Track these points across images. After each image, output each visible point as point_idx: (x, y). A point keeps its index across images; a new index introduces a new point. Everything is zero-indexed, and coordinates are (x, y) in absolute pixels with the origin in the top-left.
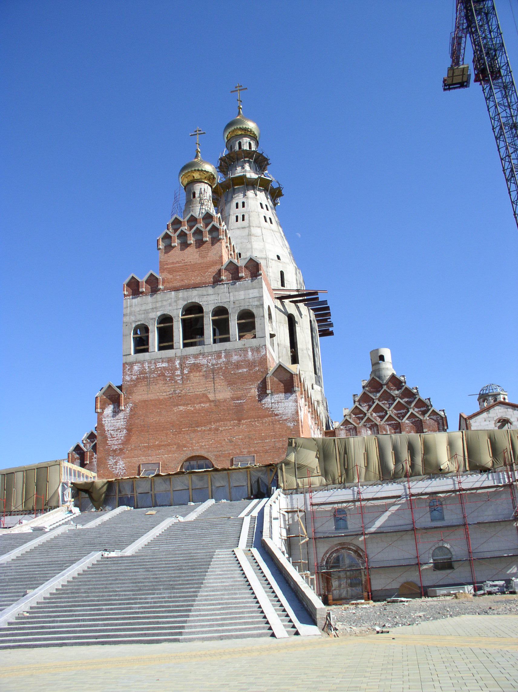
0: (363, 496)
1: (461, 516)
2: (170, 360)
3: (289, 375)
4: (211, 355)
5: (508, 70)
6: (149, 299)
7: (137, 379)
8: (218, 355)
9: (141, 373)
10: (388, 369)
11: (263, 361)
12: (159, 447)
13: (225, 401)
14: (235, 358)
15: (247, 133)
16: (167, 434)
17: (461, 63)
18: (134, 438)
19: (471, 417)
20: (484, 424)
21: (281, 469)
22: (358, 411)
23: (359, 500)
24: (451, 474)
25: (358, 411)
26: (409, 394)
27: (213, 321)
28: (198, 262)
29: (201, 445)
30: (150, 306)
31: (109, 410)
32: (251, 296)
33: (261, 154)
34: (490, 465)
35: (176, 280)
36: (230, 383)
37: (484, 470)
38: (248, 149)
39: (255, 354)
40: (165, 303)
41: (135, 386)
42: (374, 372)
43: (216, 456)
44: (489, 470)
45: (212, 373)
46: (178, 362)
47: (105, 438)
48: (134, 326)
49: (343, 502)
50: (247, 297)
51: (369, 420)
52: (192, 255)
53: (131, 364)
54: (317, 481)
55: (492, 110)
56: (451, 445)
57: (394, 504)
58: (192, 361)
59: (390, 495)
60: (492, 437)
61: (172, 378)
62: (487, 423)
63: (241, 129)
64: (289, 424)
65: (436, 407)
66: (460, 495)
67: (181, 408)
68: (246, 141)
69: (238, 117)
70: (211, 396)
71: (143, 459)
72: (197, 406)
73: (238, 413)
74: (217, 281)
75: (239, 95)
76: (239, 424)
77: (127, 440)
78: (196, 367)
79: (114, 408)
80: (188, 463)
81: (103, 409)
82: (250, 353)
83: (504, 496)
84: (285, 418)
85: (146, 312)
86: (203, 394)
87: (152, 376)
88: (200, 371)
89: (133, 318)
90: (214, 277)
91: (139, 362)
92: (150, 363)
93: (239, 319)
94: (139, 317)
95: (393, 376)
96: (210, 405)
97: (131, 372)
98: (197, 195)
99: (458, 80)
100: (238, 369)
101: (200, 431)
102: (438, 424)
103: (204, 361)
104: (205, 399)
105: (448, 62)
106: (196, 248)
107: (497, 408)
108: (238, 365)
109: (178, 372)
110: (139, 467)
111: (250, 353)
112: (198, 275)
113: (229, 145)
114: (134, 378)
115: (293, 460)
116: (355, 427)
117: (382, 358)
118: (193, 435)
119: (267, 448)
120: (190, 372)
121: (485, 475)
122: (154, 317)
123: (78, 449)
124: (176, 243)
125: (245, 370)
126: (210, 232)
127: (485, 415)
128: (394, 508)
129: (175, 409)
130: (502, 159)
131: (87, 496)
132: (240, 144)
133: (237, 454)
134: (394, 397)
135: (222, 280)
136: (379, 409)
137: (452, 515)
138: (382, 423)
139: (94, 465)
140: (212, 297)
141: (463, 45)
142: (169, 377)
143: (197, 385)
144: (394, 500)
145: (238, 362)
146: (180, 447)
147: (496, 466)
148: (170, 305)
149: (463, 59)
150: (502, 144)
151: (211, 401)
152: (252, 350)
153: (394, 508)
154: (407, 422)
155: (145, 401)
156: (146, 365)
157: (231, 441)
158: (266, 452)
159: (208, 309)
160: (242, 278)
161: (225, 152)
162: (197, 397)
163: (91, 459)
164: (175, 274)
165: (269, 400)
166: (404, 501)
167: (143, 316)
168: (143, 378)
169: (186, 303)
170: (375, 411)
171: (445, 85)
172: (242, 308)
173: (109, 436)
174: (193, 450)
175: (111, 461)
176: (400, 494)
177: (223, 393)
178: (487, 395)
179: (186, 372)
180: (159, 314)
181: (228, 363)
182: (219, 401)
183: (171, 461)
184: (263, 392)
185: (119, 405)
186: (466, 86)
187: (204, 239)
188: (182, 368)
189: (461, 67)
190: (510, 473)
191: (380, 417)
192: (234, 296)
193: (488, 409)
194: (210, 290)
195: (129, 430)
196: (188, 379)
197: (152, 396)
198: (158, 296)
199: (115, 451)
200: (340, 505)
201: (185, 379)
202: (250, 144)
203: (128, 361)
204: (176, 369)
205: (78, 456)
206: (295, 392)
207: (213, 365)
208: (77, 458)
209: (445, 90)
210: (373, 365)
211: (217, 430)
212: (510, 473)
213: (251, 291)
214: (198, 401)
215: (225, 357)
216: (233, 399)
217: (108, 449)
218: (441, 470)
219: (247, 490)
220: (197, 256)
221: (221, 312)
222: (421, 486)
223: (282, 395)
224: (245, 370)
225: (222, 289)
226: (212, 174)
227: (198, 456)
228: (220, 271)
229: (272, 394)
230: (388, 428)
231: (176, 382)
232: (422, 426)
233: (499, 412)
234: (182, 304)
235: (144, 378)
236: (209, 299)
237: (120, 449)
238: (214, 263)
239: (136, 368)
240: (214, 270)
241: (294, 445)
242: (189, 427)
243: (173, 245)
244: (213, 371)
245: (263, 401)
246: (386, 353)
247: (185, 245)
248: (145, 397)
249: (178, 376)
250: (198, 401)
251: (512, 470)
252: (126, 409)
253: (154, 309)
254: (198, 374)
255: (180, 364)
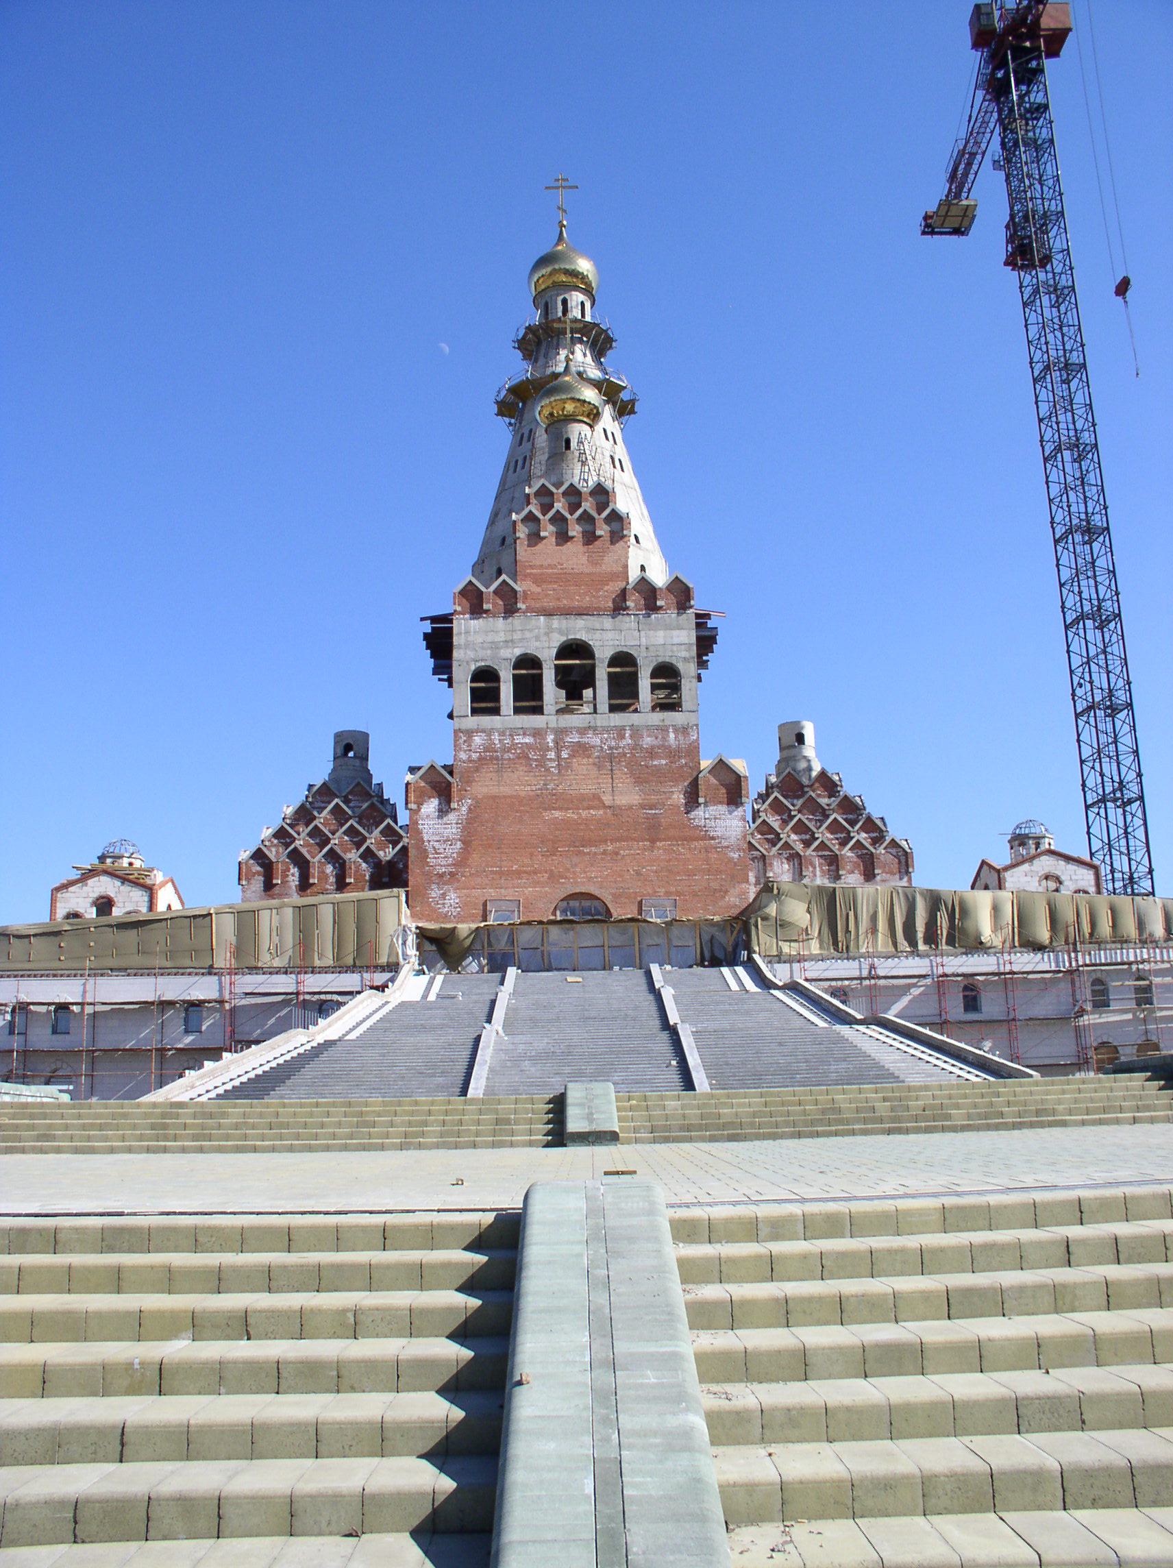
0: (881, 973)
1: (1004, 1009)
2: (538, 733)
3: (733, 777)
4: (608, 732)
5: (1067, 262)
6: (500, 623)
7: (480, 759)
8: (620, 732)
9: (486, 750)
10: (814, 756)
11: (693, 752)
12: (519, 874)
13: (630, 807)
14: (648, 741)
15: (577, 280)
16: (532, 854)
17: (964, 195)
18: (475, 858)
19: (1006, 869)
20: (1024, 879)
21: (757, 927)
22: (765, 828)
23: (870, 977)
24: (992, 950)
25: (765, 828)
26: (851, 807)
27: (610, 674)
28: (586, 571)
29: (590, 877)
30: (501, 637)
31: (431, 806)
32: (676, 641)
33: (606, 331)
34: (1047, 942)
35: (547, 595)
36: (639, 781)
37: (1039, 948)
38: (579, 317)
39: (681, 737)
40: (528, 635)
41: (477, 770)
42: (784, 762)
43: (614, 895)
44: (1045, 947)
45: (610, 759)
46: (552, 737)
47: (424, 854)
48: (473, 668)
49: (842, 979)
50: (669, 641)
51: (787, 846)
52: (574, 556)
53: (470, 733)
54: (815, 948)
55: (1033, 330)
56: (996, 909)
57: (914, 985)
58: (574, 738)
59: (901, 974)
60: (1142, 912)
61: (542, 762)
62: (1029, 879)
63: (567, 272)
64: (732, 854)
65: (894, 831)
66: (1007, 981)
67: (557, 814)
68: (576, 298)
69: (560, 248)
70: (607, 799)
71: (491, 893)
72: (584, 813)
73: (653, 831)
74: (619, 607)
75: (561, 196)
76: (652, 849)
77: (462, 861)
78: (581, 749)
79: (440, 804)
80: (565, 903)
81: (420, 804)
82: (672, 735)
83: (1062, 985)
84: (726, 844)
85: (495, 646)
86: (594, 795)
87: (506, 756)
88: (589, 757)
89: (471, 654)
90: (614, 601)
91: (483, 731)
92: (502, 733)
93: (653, 676)
94: (481, 654)
95: (823, 774)
96: (605, 813)
97: (470, 746)
98: (574, 444)
99: (953, 223)
100: (652, 758)
101: (589, 853)
102: (900, 862)
103: (596, 741)
104: (596, 802)
105: (940, 189)
106: (585, 544)
107: (1044, 858)
108: (651, 753)
109: (552, 755)
110: (485, 905)
111: (672, 735)
112: (585, 594)
113: (543, 300)
114: (475, 756)
115: (774, 914)
116: (764, 856)
117: (800, 738)
118: (575, 859)
119: (696, 888)
120: (571, 756)
121: (1039, 955)
122: (509, 656)
123: (259, 855)
124: (548, 531)
125: (664, 762)
126: (608, 520)
127: (1026, 867)
128: (916, 992)
129: (547, 815)
130: (1040, 420)
131: (434, 948)
132: (565, 302)
133: (649, 894)
134: (824, 810)
135: (627, 608)
136: (800, 828)
137: (991, 1006)
138: (809, 852)
139: (290, 887)
140: (610, 635)
141: (975, 167)
142: (536, 760)
143: (583, 779)
144: (915, 980)
145: (653, 747)
146: (553, 878)
147: (1055, 944)
148: (537, 638)
149: (970, 190)
150: (1043, 395)
151: (605, 807)
152: (676, 730)
153: (916, 992)
154: (850, 854)
155: (494, 798)
156: (496, 737)
157: (638, 873)
158: (694, 894)
159: (603, 653)
160: (660, 608)
161: (536, 318)
162: (582, 798)
163: (285, 876)
164: (544, 586)
165: (701, 813)
166: (928, 981)
167: (489, 652)
168: (489, 758)
169: (564, 639)
170: (795, 830)
171: (927, 226)
172: (660, 660)
173: (431, 850)
174: (576, 882)
175: (435, 892)
176: (924, 973)
177: (627, 795)
178: (1027, 836)
179: (564, 755)
180: (518, 652)
181: (634, 747)
182: (620, 807)
183: (542, 899)
184: (692, 797)
185: (448, 800)
186: (963, 234)
187: (598, 533)
188: (558, 747)
189: (965, 203)
190: (1073, 955)
191: (803, 841)
192: (647, 637)
193: (1031, 859)
194: (607, 622)
195: (466, 843)
196: (569, 766)
197: (505, 790)
198: (517, 621)
199: (441, 876)
200: (839, 983)
201: (563, 766)
202: (583, 304)
203: (463, 727)
204: (548, 749)
205: (259, 869)
206: (742, 804)
207: (610, 748)
208: (258, 873)
209: (924, 233)
210: (782, 749)
211: (617, 854)
212: (1073, 955)
213: (676, 633)
214: (585, 804)
215: (631, 737)
216: (643, 806)
217: (430, 872)
218: (981, 943)
219: (694, 952)
220: (584, 559)
221: (623, 660)
222: (959, 964)
223: (723, 808)
224: (664, 762)
225: (628, 622)
226: (596, 407)
227: (582, 894)
228: (624, 591)
229: (706, 804)
230: (817, 861)
231: (547, 770)
232: (873, 863)
233: (1046, 864)
234: (557, 640)
235: (492, 758)
236: (605, 638)
237: (451, 874)
238: (614, 577)
239: (478, 740)
240: (615, 587)
241: (775, 891)
242: (569, 846)
243: (542, 534)
244: (611, 758)
245: (692, 815)
246: (809, 731)
247: (563, 537)
248: (494, 791)
249: (550, 760)
250: (585, 804)
251: (1075, 951)
252: (462, 808)
253: (509, 643)
254: (585, 761)
255: (556, 742)
